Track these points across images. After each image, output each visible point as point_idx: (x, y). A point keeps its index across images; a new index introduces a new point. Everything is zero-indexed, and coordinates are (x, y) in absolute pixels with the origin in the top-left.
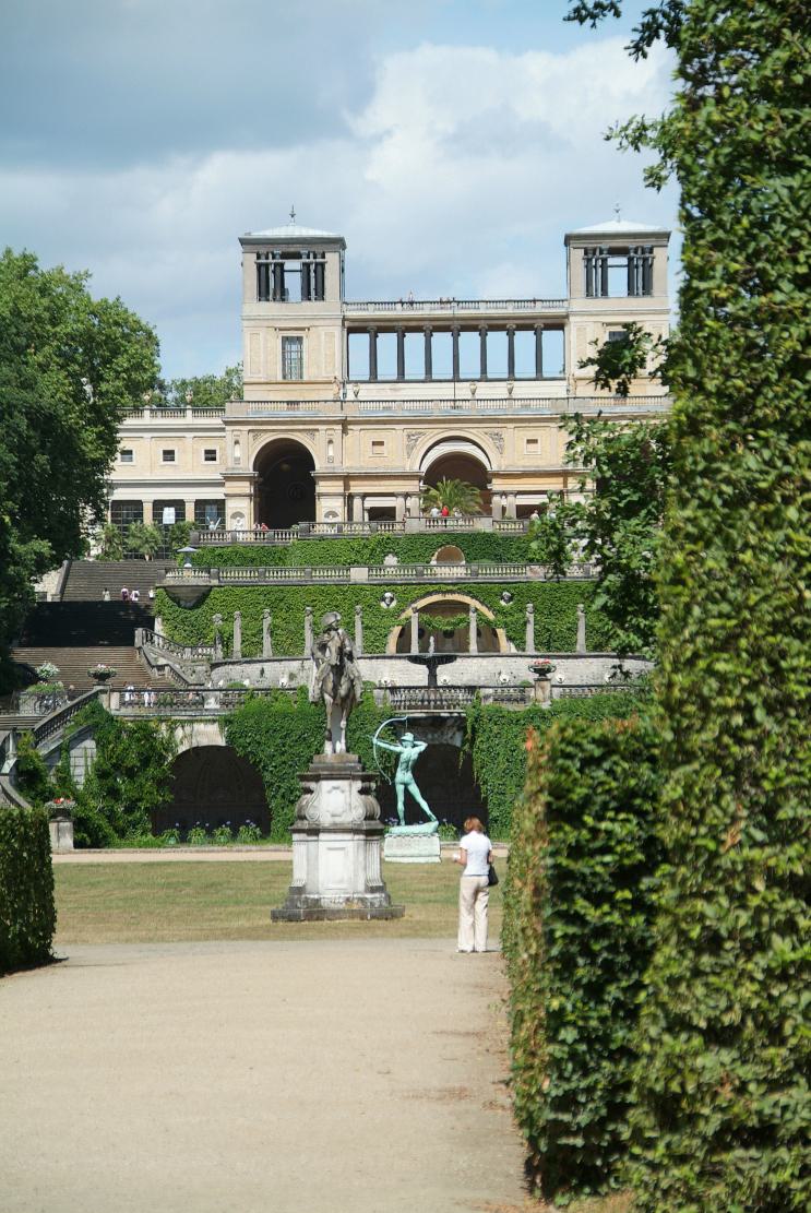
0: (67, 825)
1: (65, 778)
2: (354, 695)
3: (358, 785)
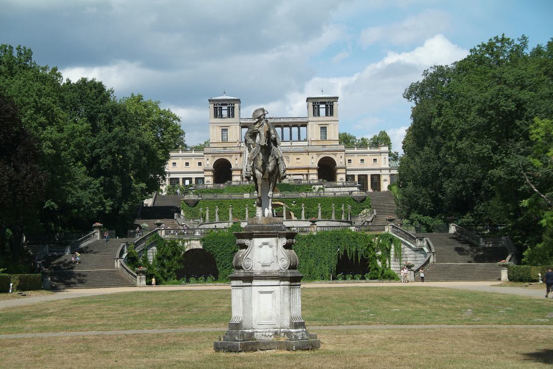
1: (146, 260)
2: (279, 172)
3: (284, 241)
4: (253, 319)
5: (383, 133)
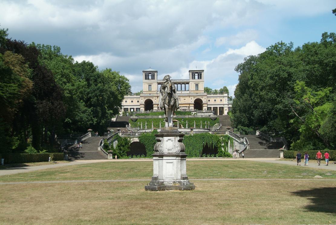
0: (111, 155)
1: (112, 147)
2: (176, 105)
3: (178, 138)
5: (225, 87)
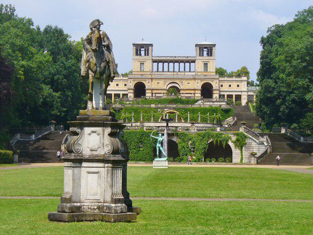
3: (108, 130)
4: (82, 194)
5: (244, 68)
